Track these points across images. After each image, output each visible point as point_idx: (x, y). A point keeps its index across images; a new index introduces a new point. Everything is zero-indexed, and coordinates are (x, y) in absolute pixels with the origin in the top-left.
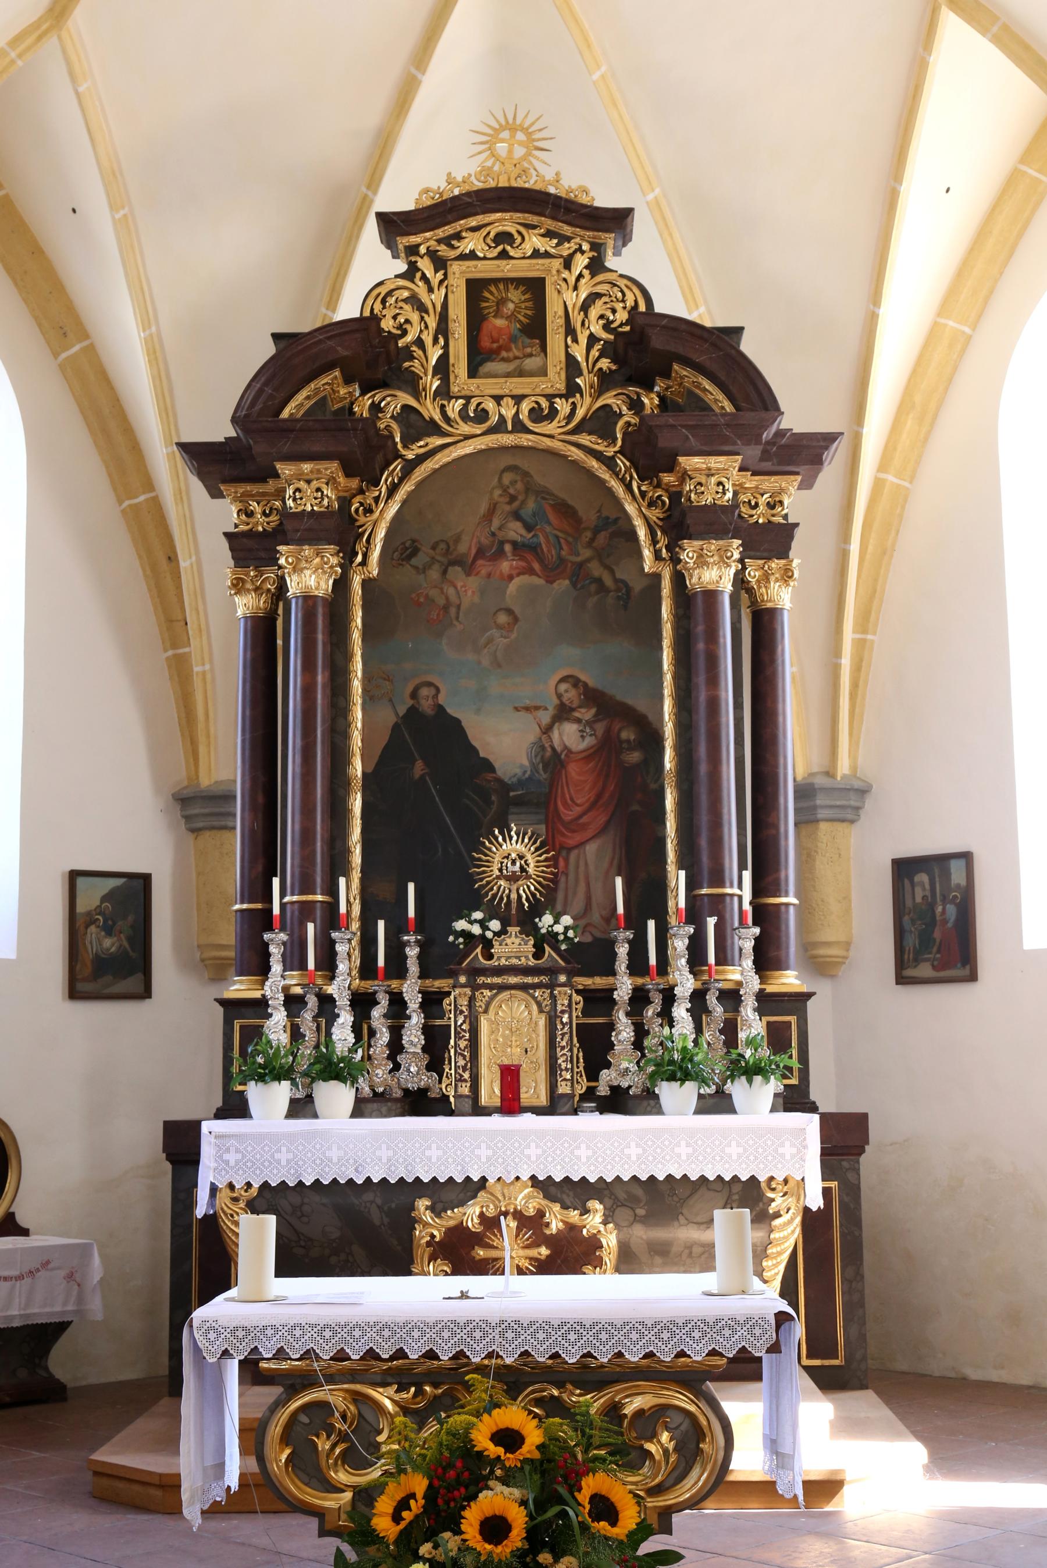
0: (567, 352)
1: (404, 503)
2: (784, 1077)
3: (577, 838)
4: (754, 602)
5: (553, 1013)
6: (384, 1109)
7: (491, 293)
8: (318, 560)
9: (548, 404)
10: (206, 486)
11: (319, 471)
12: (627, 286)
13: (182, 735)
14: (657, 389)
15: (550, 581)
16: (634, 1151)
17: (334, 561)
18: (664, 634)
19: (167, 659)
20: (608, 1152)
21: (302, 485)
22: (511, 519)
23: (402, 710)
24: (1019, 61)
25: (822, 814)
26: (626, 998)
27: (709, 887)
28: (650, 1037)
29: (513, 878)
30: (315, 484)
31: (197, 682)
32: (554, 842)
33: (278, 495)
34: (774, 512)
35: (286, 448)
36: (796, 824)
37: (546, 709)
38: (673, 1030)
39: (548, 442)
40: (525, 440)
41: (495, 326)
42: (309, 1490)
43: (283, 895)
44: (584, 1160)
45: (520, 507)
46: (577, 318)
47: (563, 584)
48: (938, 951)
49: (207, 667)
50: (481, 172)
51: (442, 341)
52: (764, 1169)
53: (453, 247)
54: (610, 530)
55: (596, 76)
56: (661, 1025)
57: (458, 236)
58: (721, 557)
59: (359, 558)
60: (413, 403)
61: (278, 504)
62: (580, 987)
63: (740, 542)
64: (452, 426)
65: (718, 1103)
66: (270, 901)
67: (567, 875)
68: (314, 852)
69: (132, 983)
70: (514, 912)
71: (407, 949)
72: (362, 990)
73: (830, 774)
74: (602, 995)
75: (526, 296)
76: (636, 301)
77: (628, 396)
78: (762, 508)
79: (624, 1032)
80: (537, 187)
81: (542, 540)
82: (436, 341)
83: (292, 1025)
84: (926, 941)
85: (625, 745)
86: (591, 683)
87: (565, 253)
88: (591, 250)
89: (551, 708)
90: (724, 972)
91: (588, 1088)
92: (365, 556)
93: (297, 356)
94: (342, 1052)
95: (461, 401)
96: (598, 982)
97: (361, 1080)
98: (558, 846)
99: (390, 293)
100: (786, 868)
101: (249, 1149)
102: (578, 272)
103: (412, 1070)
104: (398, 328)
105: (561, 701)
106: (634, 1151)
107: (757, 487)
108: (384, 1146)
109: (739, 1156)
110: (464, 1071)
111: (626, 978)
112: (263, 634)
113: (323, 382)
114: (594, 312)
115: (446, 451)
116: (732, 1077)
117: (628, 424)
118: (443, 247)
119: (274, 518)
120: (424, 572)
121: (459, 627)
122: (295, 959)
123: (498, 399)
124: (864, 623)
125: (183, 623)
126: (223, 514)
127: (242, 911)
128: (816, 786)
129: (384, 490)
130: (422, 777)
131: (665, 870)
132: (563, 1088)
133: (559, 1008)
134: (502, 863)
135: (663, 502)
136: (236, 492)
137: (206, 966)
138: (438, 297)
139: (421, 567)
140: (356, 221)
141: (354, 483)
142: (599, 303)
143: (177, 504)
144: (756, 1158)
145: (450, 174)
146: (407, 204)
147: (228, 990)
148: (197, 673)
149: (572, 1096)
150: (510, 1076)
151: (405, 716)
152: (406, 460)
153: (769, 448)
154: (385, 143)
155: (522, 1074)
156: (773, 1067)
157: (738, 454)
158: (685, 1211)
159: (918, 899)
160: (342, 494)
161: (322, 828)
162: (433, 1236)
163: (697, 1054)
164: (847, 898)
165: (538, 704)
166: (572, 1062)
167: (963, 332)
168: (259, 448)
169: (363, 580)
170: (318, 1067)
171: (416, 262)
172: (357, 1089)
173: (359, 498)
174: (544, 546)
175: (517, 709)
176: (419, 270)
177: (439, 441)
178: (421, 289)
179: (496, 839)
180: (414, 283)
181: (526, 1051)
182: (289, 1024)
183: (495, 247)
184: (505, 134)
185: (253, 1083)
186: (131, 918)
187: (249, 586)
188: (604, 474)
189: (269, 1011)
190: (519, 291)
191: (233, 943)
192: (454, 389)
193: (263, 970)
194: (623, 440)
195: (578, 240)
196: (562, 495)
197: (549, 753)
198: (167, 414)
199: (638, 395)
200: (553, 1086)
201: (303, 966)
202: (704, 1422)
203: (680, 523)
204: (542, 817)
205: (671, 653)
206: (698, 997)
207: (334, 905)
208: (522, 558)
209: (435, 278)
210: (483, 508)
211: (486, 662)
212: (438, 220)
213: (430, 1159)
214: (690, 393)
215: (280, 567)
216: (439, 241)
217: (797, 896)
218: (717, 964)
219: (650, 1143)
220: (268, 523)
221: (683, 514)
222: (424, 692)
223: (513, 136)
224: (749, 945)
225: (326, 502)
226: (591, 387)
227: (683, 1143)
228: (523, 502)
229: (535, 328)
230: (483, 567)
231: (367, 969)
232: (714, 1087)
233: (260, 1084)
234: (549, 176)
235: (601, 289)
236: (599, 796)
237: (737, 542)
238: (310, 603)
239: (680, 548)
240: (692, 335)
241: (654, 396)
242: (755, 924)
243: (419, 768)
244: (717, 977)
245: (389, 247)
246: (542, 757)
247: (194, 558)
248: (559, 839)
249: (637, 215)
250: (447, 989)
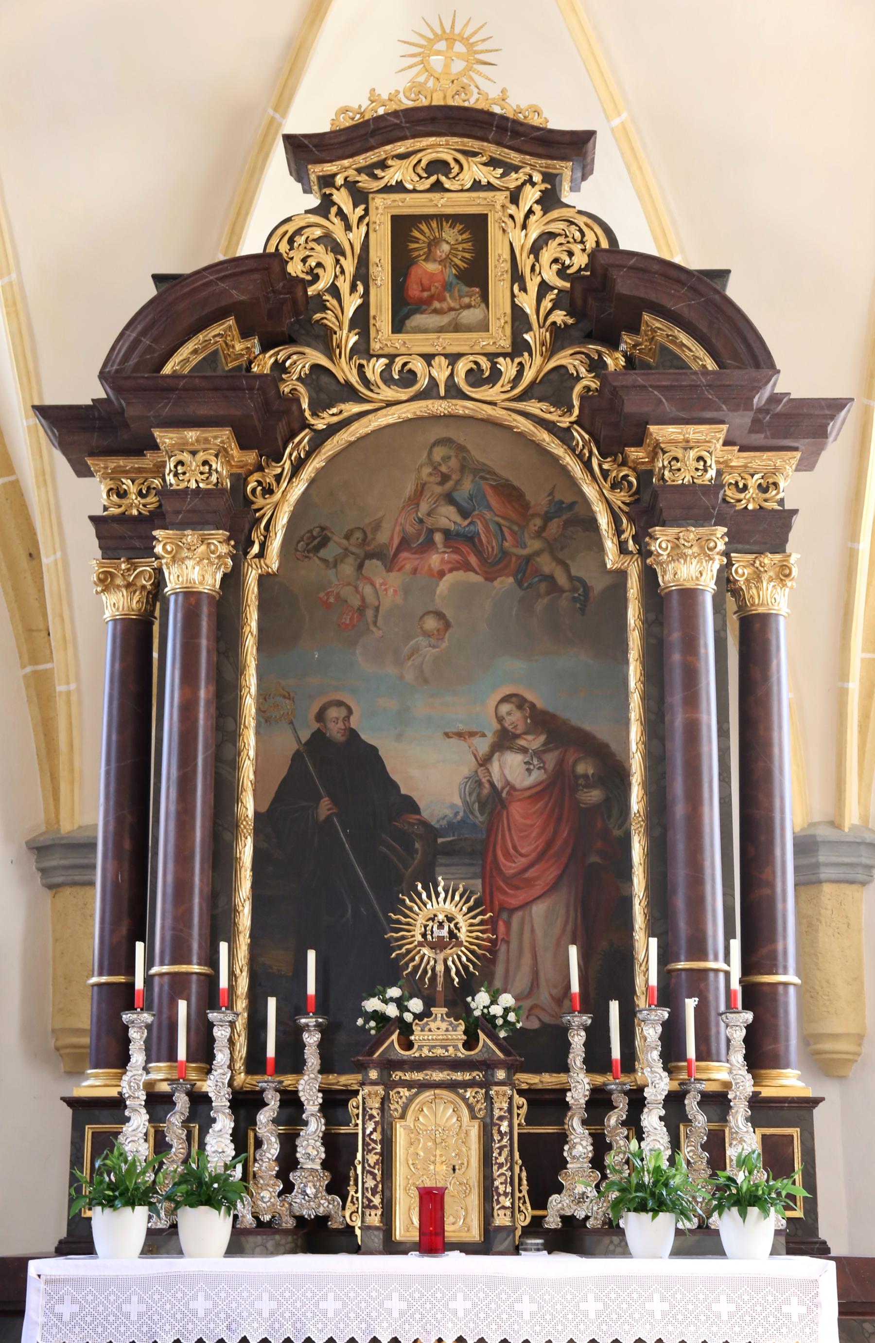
0: (514, 306)
1: (312, 482)
2: (787, 1208)
3: (523, 896)
4: (742, 607)
5: (488, 1120)
6: (270, 1244)
7: (422, 232)
8: (203, 548)
9: (489, 365)
10: (69, 461)
11: (206, 440)
12: (586, 225)
13: (41, 770)
14: (623, 347)
16: (592, 1306)
17: (223, 549)
18: (631, 644)
19: (25, 676)
20: (559, 1307)
21: (186, 457)
22: (443, 502)
25: (825, 873)
26: (583, 1101)
27: (688, 959)
28: (613, 1152)
29: (438, 945)
30: (201, 456)
31: (61, 705)
32: (492, 901)
33: (158, 472)
34: (767, 496)
35: (166, 411)
36: (796, 885)
37: (484, 735)
38: (643, 1144)
39: (489, 410)
40: (460, 407)
41: (426, 272)
43: (149, 963)
44: (527, 1317)
45: (454, 489)
46: (525, 262)
49: (73, 686)
50: (411, 88)
51: (360, 288)
52: (764, 1334)
53: (376, 177)
54: (564, 517)
56: (627, 1137)
57: (383, 165)
58: (702, 548)
59: (256, 549)
61: (157, 482)
62: (524, 1086)
63: (725, 530)
64: (372, 391)
65: (701, 1242)
66: (130, 970)
67: (508, 943)
68: (190, 911)
70: (439, 988)
71: (305, 1036)
72: (248, 1088)
73: (835, 824)
74: (552, 1096)
75: (464, 236)
77: (587, 356)
78: (752, 491)
79: (579, 1146)
80: (479, 106)
81: (480, 528)
82: (353, 288)
83: (156, 1132)
85: (581, 781)
86: (540, 704)
87: (512, 185)
88: (543, 181)
89: (490, 735)
90: (706, 1069)
91: (533, 1217)
92: (263, 546)
93: (179, 303)
94: (215, 1168)
95: (383, 361)
96: (548, 1080)
97: (239, 1205)
98: (497, 908)
99: (299, 231)
100: (785, 938)
101: (90, 1298)
102: (527, 208)
103: (308, 1191)
104: (307, 273)
105: (502, 725)
106: (592, 1306)
107: (746, 466)
108: (265, 1296)
109: (731, 1315)
110: (373, 1195)
111: (582, 1076)
112: (136, 641)
113: (213, 334)
114: (546, 255)
115: (364, 420)
116: (720, 1208)
117: (588, 388)
118: (363, 177)
119: (152, 499)
120: (335, 566)
121: (378, 634)
122: (161, 1046)
123: (428, 358)
125: (45, 634)
126: (93, 495)
127: (100, 985)
128: (819, 839)
129: (287, 466)
130: (329, 818)
131: (631, 937)
132: (501, 1219)
133: (497, 1113)
134: (426, 926)
135: (630, 484)
136: (106, 468)
137: (61, 1055)
138: (357, 236)
139: (331, 560)
140: (260, 150)
141: (251, 457)
142: (553, 244)
143: (38, 488)
144: (753, 1318)
145: (374, 90)
146: (322, 126)
147: (79, 1086)
148: (60, 693)
149: (513, 1229)
150: (432, 1201)
152: (315, 431)
153: (761, 416)
154: (297, 56)
155: (447, 1198)
156: (774, 1195)
157: (722, 422)
160: (236, 471)
161: (201, 880)
163: (675, 1176)
164: (858, 979)
165: (475, 730)
166: (512, 1184)
168: (132, 411)
169: (260, 576)
170: (184, 1187)
171: (331, 195)
172: (236, 1217)
173: (256, 476)
174: (483, 536)
175: (447, 735)
176: (334, 204)
178: (337, 228)
179: (419, 896)
180: (328, 219)
181: (454, 1170)
182: (152, 1131)
183: (427, 178)
185: (98, 1209)
188: (556, 448)
189: (127, 1113)
190: (456, 230)
191: (89, 1027)
192: (375, 346)
193: (122, 1061)
195: (528, 169)
196: (506, 474)
197: (487, 789)
198: (29, 379)
200: (487, 1216)
201: (172, 1056)
203: (650, 506)
204: (478, 870)
205: (639, 668)
206: (674, 1102)
207: (212, 980)
208: (456, 551)
210: (409, 489)
211: (409, 677)
212: (358, 145)
213: (325, 1313)
214: (664, 349)
215: (158, 558)
216: (359, 171)
217: (798, 974)
218: (699, 1058)
219: (613, 1296)
220: (144, 506)
221: (655, 496)
222: (333, 713)
224: (739, 1035)
226: (543, 344)
227: (657, 1297)
228: (458, 482)
229: (475, 275)
231: (255, 1061)
232: (696, 1220)
233: (108, 1211)
234: (493, 92)
236: (549, 845)
237: (722, 530)
238: (192, 600)
239: (651, 537)
240: (666, 276)
241: (618, 355)
242: (745, 1007)
243: (325, 808)
244: (698, 1076)
245: (299, 179)
246: (479, 795)
247: (59, 554)
248: (499, 897)
249: (599, 138)
250: (356, 1087)
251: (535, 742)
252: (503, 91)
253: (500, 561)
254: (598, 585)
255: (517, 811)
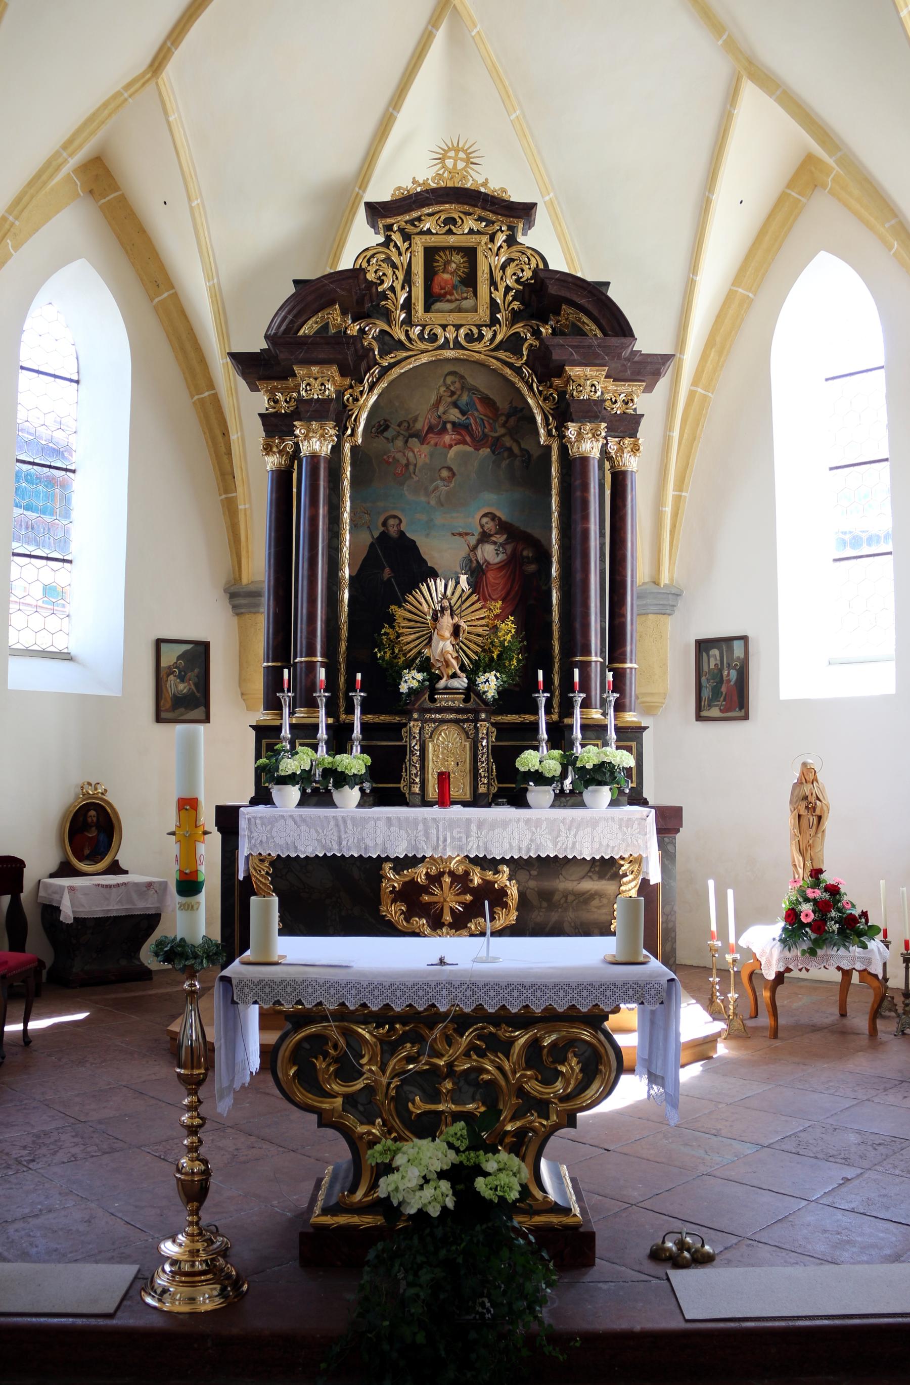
0: (491, 296)
7: (441, 257)
15: (477, 449)
17: (332, 432)
19: (222, 500)
23: (376, 534)
24: (793, 115)
42: (310, 1096)
46: (498, 275)
47: (485, 451)
48: (724, 700)
53: (415, 226)
55: (513, 117)
59: (349, 432)
60: (387, 328)
69: (198, 713)
73: (656, 583)
76: (537, 265)
77: (531, 327)
81: (472, 421)
82: (403, 288)
84: (716, 692)
86: (503, 518)
88: (508, 230)
89: (476, 534)
91: (499, 788)
93: (311, 295)
95: (419, 328)
99: (373, 256)
112: (282, 481)
114: (509, 271)
117: (531, 345)
119: (293, 403)
124: (680, 485)
126: (260, 401)
130: (389, 579)
132: (482, 789)
133: (480, 736)
135: (554, 398)
141: (347, 381)
142: (513, 265)
146: (386, 197)
150: (444, 778)
151: (378, 538)
158: (563, 873)
159: (712, 666)
160: (338, 388)
162: (394, 887)
167: (748, 297)
168: (282, 356)
169: (352, 447)
173: (350, 391)
175: (453, 534)
177: (405, 354)
184: (452, 154)
186: (196, 671)
187: (275, 449)
188: (516, 380)
192: (415, 320)
194: (528, 356)
196: (486, 392)
199: (538, 326)
200: (475, 788)
202: (602, 1051)
203: (564, 411)
208: (459, 434)
209: (403, 246)
210: (433, 399)
214: (574, 324)
215: (296, 436)
221: (568, 405)
222: (391, 522)
223: (457, 155)
225: (327, 393)
226: (507, 320)
229: (470, 280)
230: (433, 439)
235: (515, 255)
237: (604, 425)
240: (577, 285)
243: (387, 573)
251: (501, 539)
252: (487, 180)
253: (482, 440)
254: (536, 453)
255: (491, 576)
